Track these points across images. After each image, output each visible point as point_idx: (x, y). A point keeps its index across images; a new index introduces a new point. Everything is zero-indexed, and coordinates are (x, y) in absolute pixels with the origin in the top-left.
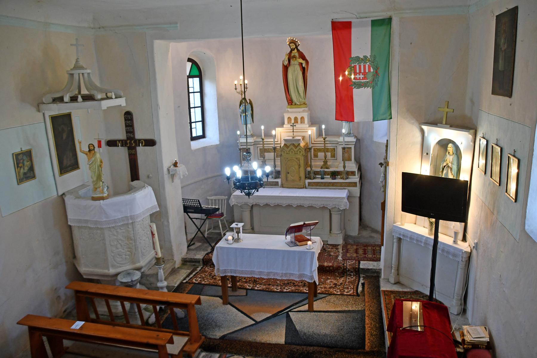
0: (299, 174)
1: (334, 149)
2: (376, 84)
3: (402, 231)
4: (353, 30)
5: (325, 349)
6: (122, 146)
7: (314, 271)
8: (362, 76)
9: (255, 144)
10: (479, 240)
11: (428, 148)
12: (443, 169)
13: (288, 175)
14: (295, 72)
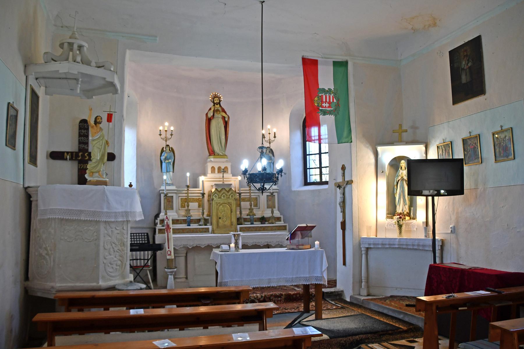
0: (231, 220)
1: (257, 198)
2: (338, 113)
3: (372, 240)
4: (320, 67)
5: (369, 335)
6: (71, 159)
7: (324, 271)
8: (327, 105)
9: (177, 192)
10: (457, 222)
11: (383, 167)
12: (397, 183)
13: (220, 221)
14: (217, 125)
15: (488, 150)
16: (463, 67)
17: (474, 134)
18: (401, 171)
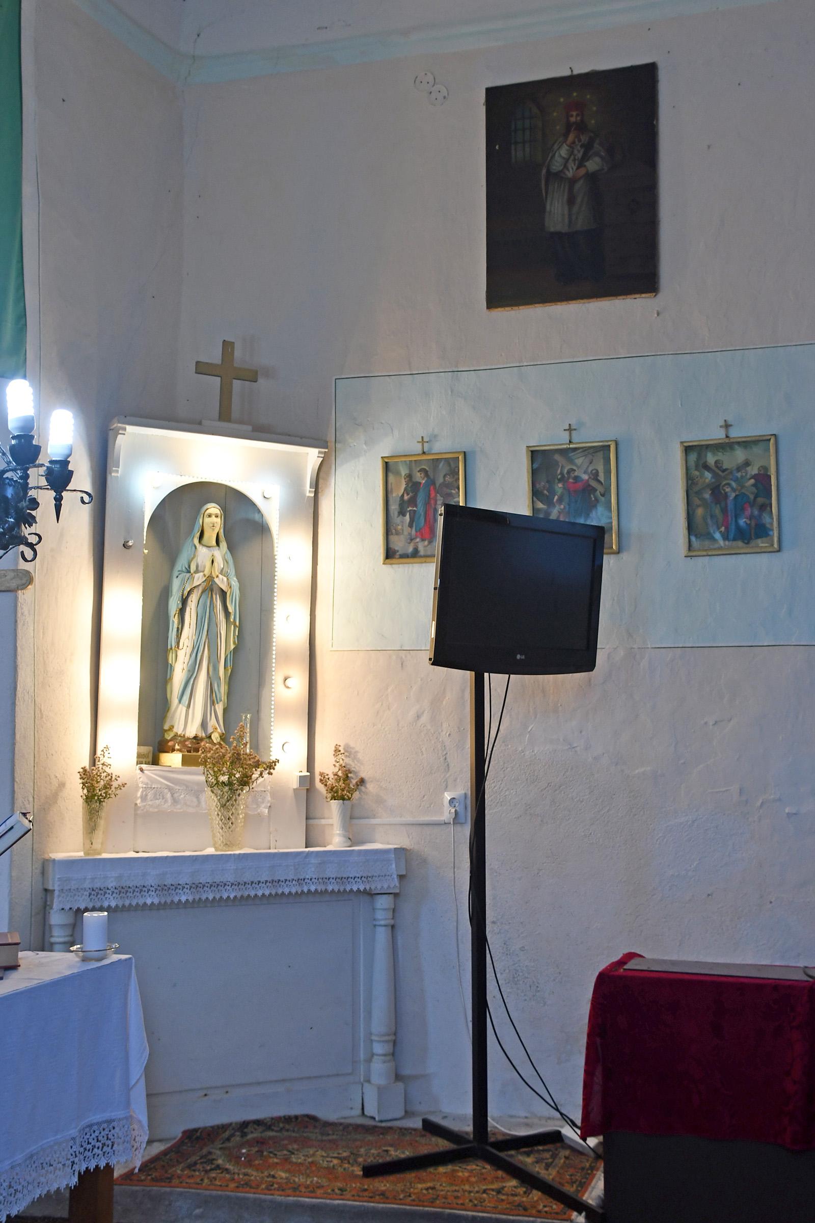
11: (130, 518)
12: (184, 602)
15: (651, 509)
16: (557, 166)
17: (589, 436)
18: (202, 551)
